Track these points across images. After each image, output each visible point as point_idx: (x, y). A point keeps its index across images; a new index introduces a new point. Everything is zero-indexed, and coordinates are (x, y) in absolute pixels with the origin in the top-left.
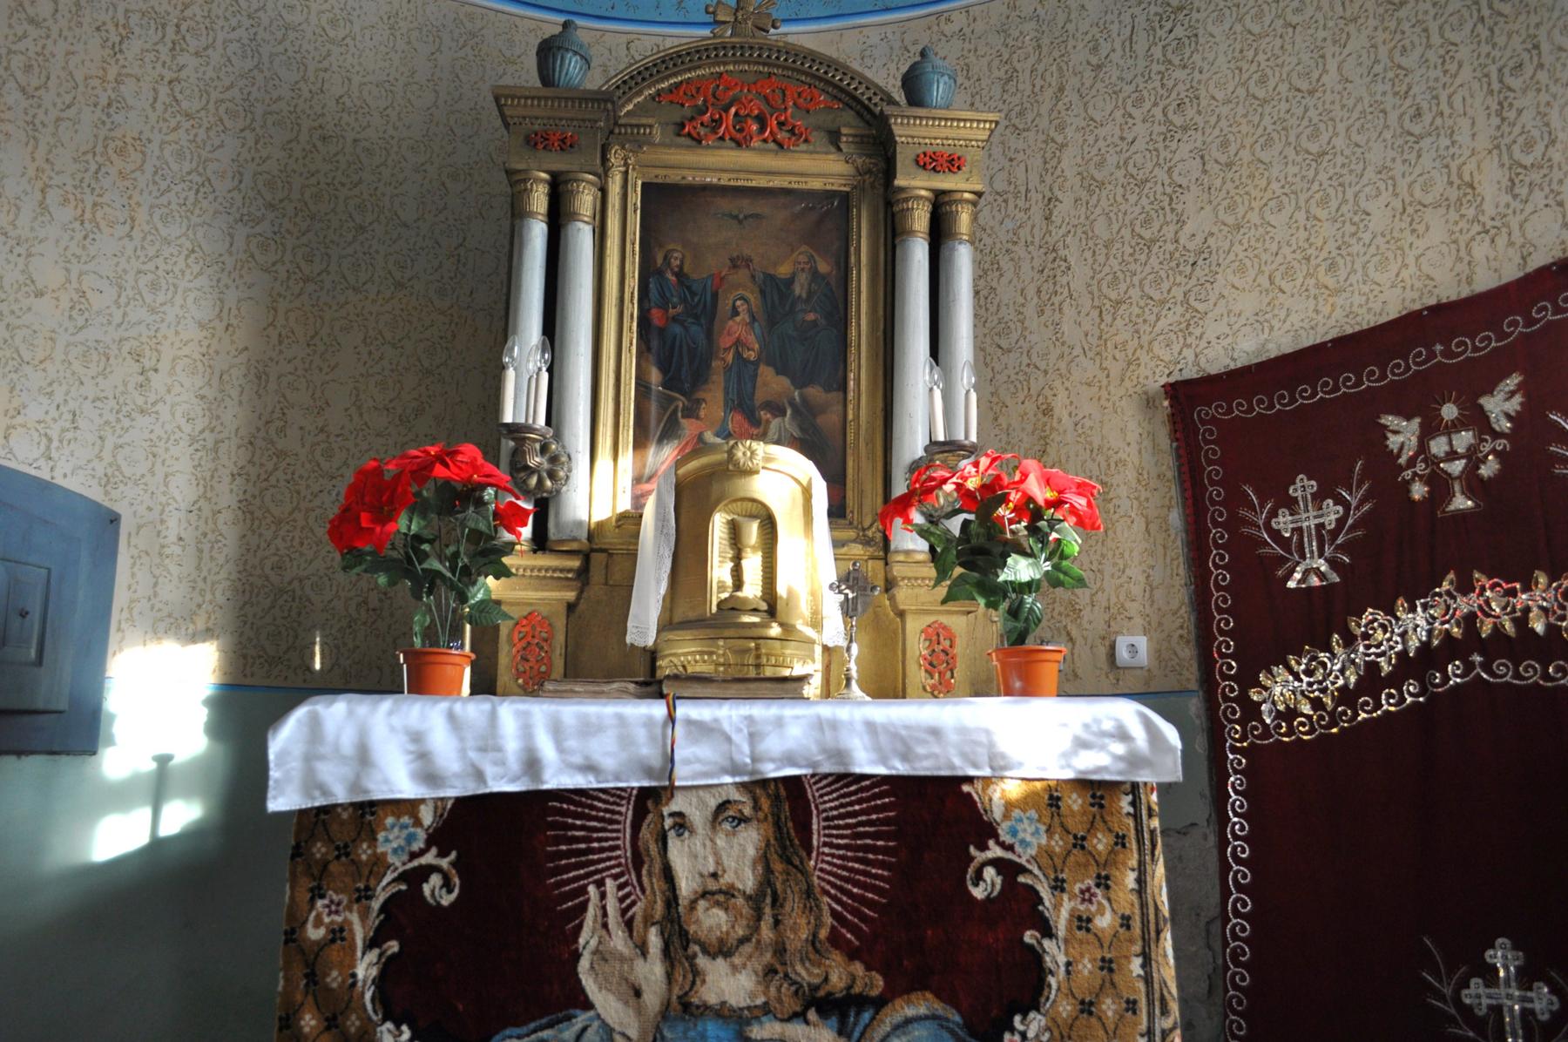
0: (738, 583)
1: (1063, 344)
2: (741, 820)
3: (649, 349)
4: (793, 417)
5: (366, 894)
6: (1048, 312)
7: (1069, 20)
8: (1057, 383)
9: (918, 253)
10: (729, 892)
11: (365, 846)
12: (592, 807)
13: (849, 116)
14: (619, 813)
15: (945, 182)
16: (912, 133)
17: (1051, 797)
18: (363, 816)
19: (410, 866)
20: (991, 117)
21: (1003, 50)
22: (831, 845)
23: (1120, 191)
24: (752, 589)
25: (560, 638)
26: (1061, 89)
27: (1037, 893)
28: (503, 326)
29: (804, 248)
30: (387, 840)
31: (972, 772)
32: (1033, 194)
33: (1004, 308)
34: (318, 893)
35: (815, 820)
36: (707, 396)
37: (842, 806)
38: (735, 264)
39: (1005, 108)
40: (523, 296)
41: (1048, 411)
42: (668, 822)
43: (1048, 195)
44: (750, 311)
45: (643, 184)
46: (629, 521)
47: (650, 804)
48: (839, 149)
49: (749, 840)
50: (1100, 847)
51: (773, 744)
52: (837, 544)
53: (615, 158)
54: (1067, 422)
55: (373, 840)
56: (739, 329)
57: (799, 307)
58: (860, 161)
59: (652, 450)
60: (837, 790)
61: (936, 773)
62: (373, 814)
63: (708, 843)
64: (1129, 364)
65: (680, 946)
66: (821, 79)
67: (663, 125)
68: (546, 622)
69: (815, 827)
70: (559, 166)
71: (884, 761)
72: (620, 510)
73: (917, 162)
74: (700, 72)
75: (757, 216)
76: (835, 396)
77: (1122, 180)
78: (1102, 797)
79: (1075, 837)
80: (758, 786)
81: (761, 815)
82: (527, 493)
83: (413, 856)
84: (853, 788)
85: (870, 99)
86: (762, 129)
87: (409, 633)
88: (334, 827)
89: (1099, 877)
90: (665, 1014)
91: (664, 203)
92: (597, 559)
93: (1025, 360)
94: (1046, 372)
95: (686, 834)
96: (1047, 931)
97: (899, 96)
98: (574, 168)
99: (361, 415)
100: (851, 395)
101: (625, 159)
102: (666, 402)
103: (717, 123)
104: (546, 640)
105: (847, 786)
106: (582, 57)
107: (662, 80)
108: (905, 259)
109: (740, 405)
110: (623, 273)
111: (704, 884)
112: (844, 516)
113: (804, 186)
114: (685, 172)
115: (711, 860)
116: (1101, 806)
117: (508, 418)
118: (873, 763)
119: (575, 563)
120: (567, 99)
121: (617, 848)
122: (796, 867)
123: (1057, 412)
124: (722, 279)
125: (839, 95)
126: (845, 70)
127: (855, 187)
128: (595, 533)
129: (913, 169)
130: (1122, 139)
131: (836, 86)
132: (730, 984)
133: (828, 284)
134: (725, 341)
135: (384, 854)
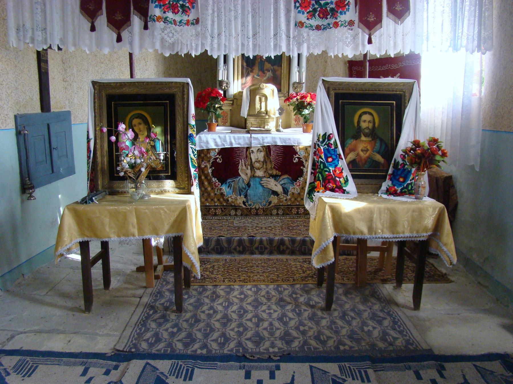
0: (261, 108)
2: (261, 151)
5: (209, 161)
10: (259, 161)
24: (263, 109)
25: (229, 116)
34: (203, 161)
36: (255, 68)
41: (326, 62)
46: (241, 93)
51: (266, 141)
52: (279, 97)
54: (330, 65)
59: (244, 78)
65: (252, 168)
71: (282, 143)
76: (280, 68)
80: (263, 147)
82: (222, 89)
90: (251, 177)
92: (235, 101)
96: (304, 167)
102: (247, 69)
119: (232, 102)
128: (234, 96)
132: (259, 173)
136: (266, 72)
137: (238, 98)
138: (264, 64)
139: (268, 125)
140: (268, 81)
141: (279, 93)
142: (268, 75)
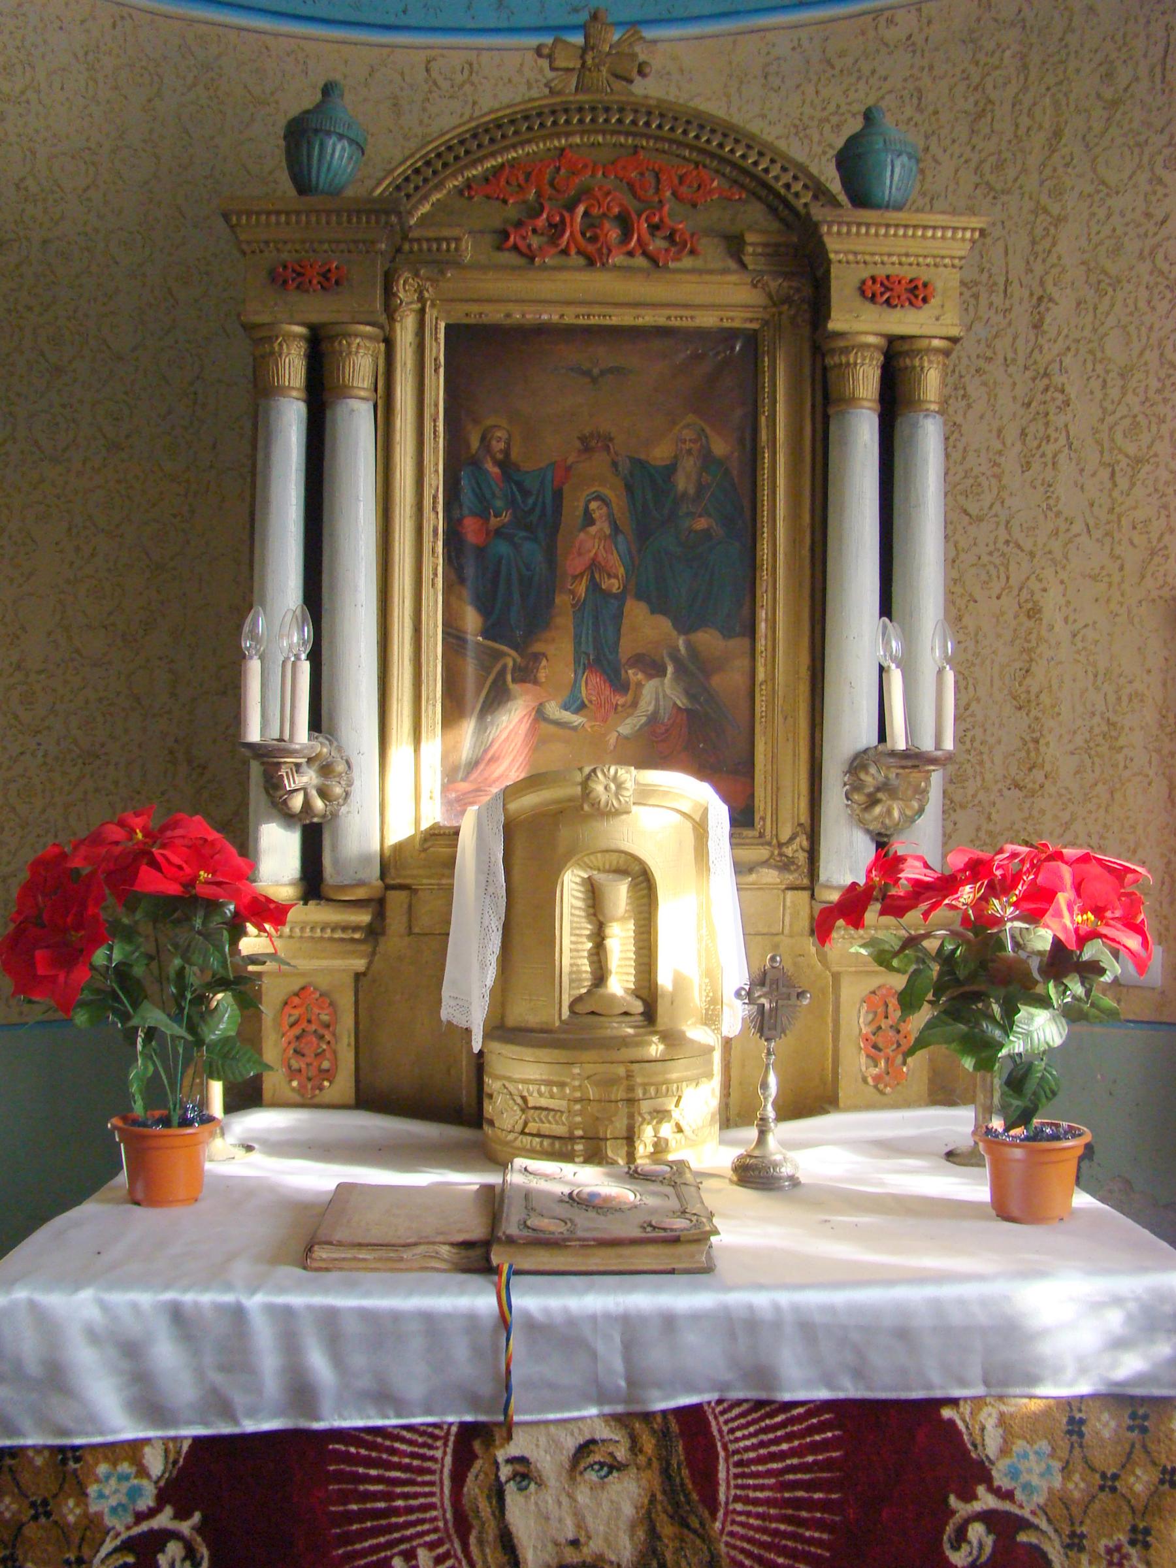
0: (600, 977)
1: (1058, 514)
2: (614, 1466)
3: (462, 580)
6: (1036, 466)
7: (1069, 29)
8: (1049, 573)
9: (863, 432)
11: (71, 1503)
12: (393, 1451)
13: (755, 213)
14: (433, 1459)
15: (905, 322)
16: (856, 248)
17: (1071, 1420)
18: (64, 1462)
19: (136, 1530)
22: (747, 1500)
23: (1143, 294)
25: (347, 1021)
26: (1057, 134)
27: (1044, 1555)
28: (244, 591)
29: (690, 418)
30: (101, 1495)
31: (956, 1393)
32: (1015, 288)
33: (971, 455)
35: (722, 1466)
36: (550, 650)
37: (762, 1444)
38: (588, 445)
39: (975, 158)
41: (1034, 613)
42: (505, 1472)
43: (1038, 292)
45: (447, 327)
46: (443, 838)
47: (477, 1446)
48: (743, 266)
49: (626, 1495)
50: (1138, 1487)
52: (741, 868)
53: (405, 292)
54: (1061, 631)
55: (82, 1494)
56: (595, 544)
58: (774, 285)
59: (468, 728)
60: (754, 1422)
61: (904, 1395)
62: (77, 1460)
63: (565, 1500)
64: (1153, 553)
66: (712, 155)
68: (326, 999)
69: (722, 1475)
70: (314, 318)
72: (425, 825)
73: (863, 293)
74: (529, 149)
75: (616, 371)
77: (1146, 278)
78: (1145, 1417)
79: (1104, 1476)
81: (642, 1459)
83: (140, 1517)
84: (778, 1419)
85: (788, 186)
86: (626, 235)
87: (128, 1098)
88: (26, 1477)
89: (1134, 1529)
91: (481, 355)
92: (397, 900)
93: (1003, 535)
94: (1032, 555)
95: (532, 1486)
97: (835, 186)
99: (70, 638)
100: (761, 644)
103: (557, 229)
104: (327, 1026)
105: (770, 1415)
106: (352, 141)
107: (474, 164)
108: (844, 442)
109: (598, 660)
110: (423, 465)
111: (560, 1554)
112: (750, 823)
114: (511, 307)
115: (569, 1522)
116: (1144, 1430)
117: (254, 734)
118: (809, 1384)
119: (364, 918)
120: (328, 212)
121: (432, 1506)
122: (695, 1532)
123: (1047, 615)
124: (568, 469)
126: (750, 141)
127: (766, 323)
129: (858, 301)
130: (1148, 215)
131: (734, 165)
134: (575, 564)
135: (99, 1515)
137: (412, 883)
138: (618, 617)
139: (661, 1115)
140: (658, 748)
141: (735, 841)
142: (647, 704)
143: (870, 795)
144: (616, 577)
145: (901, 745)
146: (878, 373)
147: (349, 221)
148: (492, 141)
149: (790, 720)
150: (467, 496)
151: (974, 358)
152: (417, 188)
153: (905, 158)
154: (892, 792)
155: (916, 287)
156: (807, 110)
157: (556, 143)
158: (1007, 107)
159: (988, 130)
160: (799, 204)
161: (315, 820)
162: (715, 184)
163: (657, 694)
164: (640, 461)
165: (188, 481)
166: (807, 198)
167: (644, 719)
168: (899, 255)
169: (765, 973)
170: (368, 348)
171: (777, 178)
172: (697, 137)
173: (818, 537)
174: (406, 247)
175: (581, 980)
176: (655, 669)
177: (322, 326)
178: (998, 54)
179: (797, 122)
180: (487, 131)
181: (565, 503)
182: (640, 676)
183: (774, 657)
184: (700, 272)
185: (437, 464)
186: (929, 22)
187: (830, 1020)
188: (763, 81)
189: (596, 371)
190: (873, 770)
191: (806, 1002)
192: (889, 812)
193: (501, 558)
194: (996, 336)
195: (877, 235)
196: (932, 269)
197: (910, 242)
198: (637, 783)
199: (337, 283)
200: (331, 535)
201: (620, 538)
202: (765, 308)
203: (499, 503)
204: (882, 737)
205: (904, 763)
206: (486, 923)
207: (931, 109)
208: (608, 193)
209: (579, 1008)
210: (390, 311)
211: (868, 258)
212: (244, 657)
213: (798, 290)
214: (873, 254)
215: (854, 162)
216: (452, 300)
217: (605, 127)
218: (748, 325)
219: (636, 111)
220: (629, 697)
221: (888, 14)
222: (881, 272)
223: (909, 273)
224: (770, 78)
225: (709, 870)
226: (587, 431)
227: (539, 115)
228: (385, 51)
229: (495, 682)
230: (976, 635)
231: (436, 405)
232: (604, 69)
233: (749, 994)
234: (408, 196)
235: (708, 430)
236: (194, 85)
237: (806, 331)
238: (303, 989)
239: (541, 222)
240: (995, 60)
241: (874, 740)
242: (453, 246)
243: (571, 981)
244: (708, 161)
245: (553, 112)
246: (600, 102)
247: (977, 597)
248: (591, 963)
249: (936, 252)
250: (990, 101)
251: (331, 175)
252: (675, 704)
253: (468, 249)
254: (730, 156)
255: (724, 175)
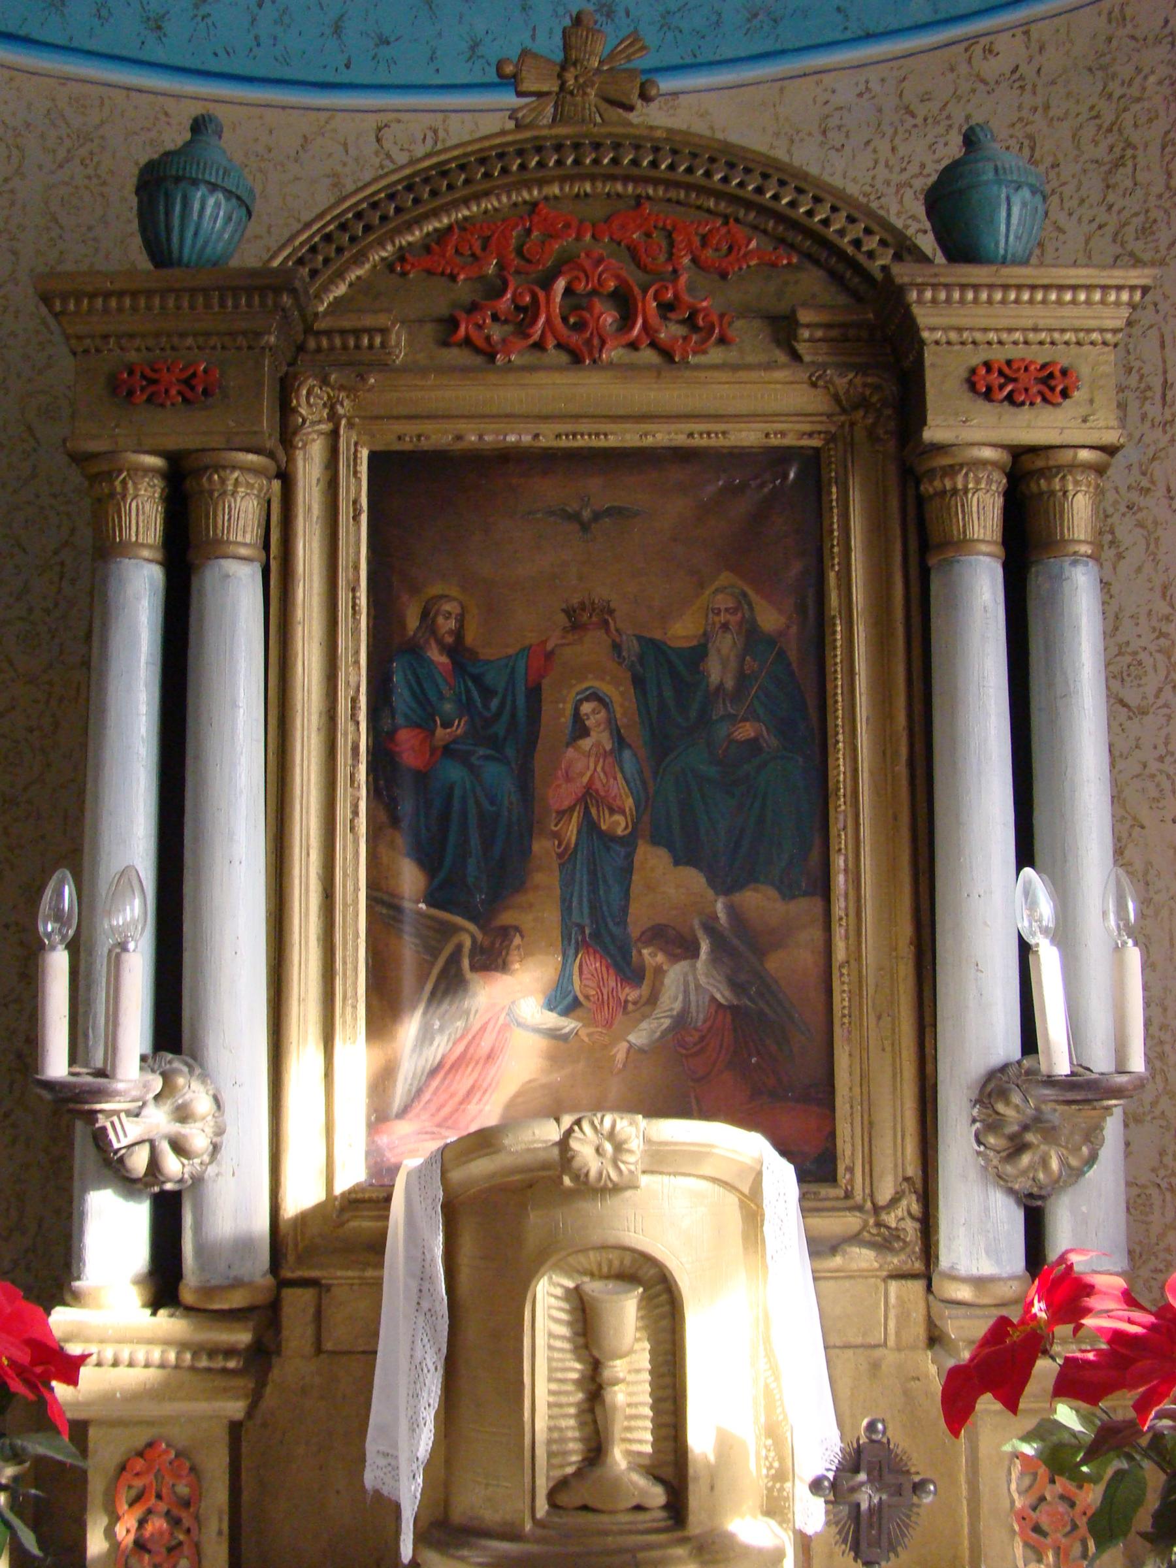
0: (596, 1450)
4: (715, 959)
9: (982, 588)
13: (812, 281)
15: (1036, 426)
20: (1137, 277)
21: (1103, 105)
24: (633, 1437)
25: (217, 1495)
36: (526, 920)
38: (577, 620)
39: (1113, 221)
40: (112, 734)
44: (613, 726)
45: (373, 456)
46: (370, 1202)
48: (796, 357)
52: (820, 1247)
53: (310, 407)
56: (589, 765)
57: (719, 711)
58: (841, 383)
59: (410, 1028)
66: (749, 205)
67: (413, 323)
72: (340, 1188)
73: (972, 386)
76: (806, 907)
85: (857, 243)
91: (419, 494)
92: (297, 1303)
97: (927, 243)
98: (216, 441)
100: (839, 907)
101: (331, 406)
103: (526, 314)
106: (229, 194)
107: (409, 226)
109: (596, 935)
113: (721, 442)
114: (462, 426)
119: (242, 1337)
120: (193, 291)
124: (549, 656)
125: (791, 236)
127: (831, 438)
131: (780, 218)
133: (781, 654)
134: (560, 794)
136: (651, 957)
138: (627, 871)
142: (671, 999)
143: (1012, 1138)
144: (623, 813)
145: (1062, 1067)
146: (999, 501)
147: (222, 304)
148: (434, 193)
149: (886, 1020)
150: (402, 696)
151: (1123, 490)
152: (326, 261)
153: (1025, 193)
154: (1050, 1134)
155: (1051, 376)
156: (881, 172)
157: (526, 195)
158: (1154, 149)
159: (1129, 183)
160: (874, 267)
161: (169, 1186)
162: (753, 244)
163: (686, 984)
164: (652, 642)
165: (51, 683)
166: (885, 258)
167: (667, 1022)
168: (1024, 330)
169: (859, 1451)
170: (249, 486)
171: (841, 233)
172: (725, 180)
173: (919, 746)
174: (312, 344)
175: (565, 1453)
176: (685, 948)
177: (188, 453)
178: (1138, 80)
179: (868, 189)
180: (426, 180)
181: (545, 707)
182: (660, 958)
183: (859, 943)
184: (735, 368)
185: (357, 652)
186: (1041, 49)
187: (962, 1478)
188: (821, 138)
189: (586, 514)
190: (1016, 1098)
191: (928, 1500)
192: (1044, 1162)
193: (451, 788)
194: (1153, 459)
195: (990, 301)
196: (1074, 349)
197: (1039, 310)
198: (647, 1141)
199: (206, 393)
200: (197, 757)
201: (627, 754)
202: (829, 416)
203: (448, 707)
204: (1029, 1040)
205: (1070, 1096)
206: (419, 1354)
207: (1048, 161)
208: (600, 261)
209: (563, 1499)
210: (288, 435)
211: (979, 336)
212: (42, 947)
213: (877, 388)
214: (985, 330)
215: (954, 212)
216: (377, 418)
217: (596, 170)
218: (805, 442)
219: (637, 148)
220: (645, 989)
221: (984, 41)
222: (998, 355)
223: (1041, 356)
224: (830, 135)
225: (765, 1266)
226: (575, 601)
227: (501, 156)
228: (324, 115)
229: (444, 972)
230: (1146, 873)
231: (356, 568)
232: (592, 92)
233: (834, 1485)
234: (314, 273)
235: (750, 592)
236: (68, 160)
237: (891, 446)
238: (151, 1445)
239: (505, 303)
240: (1134, 91)
241: (1015, 1052)
242: (378, 340)
243: (551, 1455)
244: (741, 213)
245: (520, 153)
246: (585, 136)
247: (1146, 822)
248: (582, 1425)
249: (1077, 323)
250: (1129, 145)
251: (200, 242)
252: (713, 999)
253: (400, 345)
254: (773, 204)
255: (765, 232)
